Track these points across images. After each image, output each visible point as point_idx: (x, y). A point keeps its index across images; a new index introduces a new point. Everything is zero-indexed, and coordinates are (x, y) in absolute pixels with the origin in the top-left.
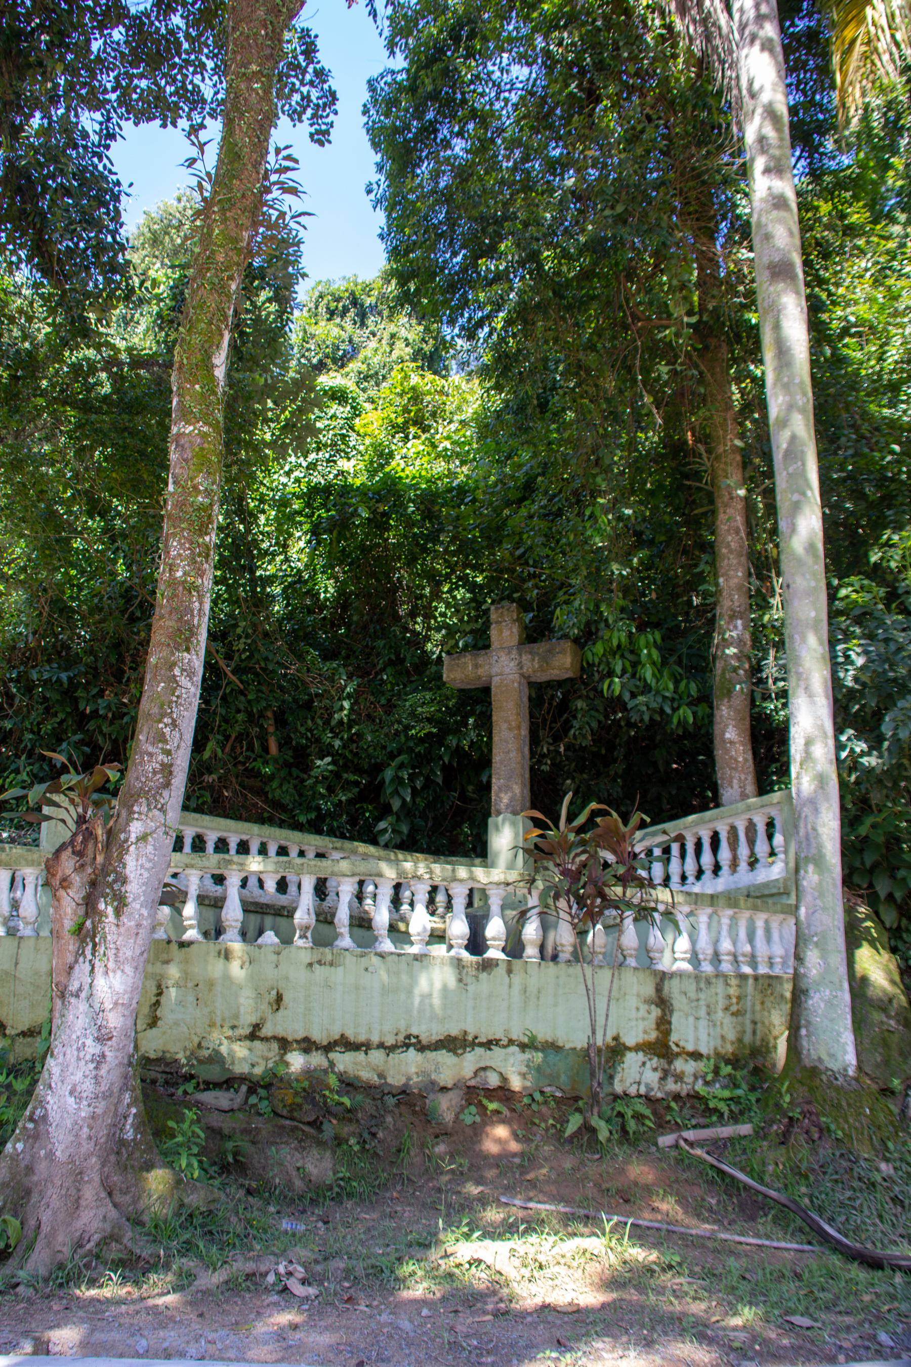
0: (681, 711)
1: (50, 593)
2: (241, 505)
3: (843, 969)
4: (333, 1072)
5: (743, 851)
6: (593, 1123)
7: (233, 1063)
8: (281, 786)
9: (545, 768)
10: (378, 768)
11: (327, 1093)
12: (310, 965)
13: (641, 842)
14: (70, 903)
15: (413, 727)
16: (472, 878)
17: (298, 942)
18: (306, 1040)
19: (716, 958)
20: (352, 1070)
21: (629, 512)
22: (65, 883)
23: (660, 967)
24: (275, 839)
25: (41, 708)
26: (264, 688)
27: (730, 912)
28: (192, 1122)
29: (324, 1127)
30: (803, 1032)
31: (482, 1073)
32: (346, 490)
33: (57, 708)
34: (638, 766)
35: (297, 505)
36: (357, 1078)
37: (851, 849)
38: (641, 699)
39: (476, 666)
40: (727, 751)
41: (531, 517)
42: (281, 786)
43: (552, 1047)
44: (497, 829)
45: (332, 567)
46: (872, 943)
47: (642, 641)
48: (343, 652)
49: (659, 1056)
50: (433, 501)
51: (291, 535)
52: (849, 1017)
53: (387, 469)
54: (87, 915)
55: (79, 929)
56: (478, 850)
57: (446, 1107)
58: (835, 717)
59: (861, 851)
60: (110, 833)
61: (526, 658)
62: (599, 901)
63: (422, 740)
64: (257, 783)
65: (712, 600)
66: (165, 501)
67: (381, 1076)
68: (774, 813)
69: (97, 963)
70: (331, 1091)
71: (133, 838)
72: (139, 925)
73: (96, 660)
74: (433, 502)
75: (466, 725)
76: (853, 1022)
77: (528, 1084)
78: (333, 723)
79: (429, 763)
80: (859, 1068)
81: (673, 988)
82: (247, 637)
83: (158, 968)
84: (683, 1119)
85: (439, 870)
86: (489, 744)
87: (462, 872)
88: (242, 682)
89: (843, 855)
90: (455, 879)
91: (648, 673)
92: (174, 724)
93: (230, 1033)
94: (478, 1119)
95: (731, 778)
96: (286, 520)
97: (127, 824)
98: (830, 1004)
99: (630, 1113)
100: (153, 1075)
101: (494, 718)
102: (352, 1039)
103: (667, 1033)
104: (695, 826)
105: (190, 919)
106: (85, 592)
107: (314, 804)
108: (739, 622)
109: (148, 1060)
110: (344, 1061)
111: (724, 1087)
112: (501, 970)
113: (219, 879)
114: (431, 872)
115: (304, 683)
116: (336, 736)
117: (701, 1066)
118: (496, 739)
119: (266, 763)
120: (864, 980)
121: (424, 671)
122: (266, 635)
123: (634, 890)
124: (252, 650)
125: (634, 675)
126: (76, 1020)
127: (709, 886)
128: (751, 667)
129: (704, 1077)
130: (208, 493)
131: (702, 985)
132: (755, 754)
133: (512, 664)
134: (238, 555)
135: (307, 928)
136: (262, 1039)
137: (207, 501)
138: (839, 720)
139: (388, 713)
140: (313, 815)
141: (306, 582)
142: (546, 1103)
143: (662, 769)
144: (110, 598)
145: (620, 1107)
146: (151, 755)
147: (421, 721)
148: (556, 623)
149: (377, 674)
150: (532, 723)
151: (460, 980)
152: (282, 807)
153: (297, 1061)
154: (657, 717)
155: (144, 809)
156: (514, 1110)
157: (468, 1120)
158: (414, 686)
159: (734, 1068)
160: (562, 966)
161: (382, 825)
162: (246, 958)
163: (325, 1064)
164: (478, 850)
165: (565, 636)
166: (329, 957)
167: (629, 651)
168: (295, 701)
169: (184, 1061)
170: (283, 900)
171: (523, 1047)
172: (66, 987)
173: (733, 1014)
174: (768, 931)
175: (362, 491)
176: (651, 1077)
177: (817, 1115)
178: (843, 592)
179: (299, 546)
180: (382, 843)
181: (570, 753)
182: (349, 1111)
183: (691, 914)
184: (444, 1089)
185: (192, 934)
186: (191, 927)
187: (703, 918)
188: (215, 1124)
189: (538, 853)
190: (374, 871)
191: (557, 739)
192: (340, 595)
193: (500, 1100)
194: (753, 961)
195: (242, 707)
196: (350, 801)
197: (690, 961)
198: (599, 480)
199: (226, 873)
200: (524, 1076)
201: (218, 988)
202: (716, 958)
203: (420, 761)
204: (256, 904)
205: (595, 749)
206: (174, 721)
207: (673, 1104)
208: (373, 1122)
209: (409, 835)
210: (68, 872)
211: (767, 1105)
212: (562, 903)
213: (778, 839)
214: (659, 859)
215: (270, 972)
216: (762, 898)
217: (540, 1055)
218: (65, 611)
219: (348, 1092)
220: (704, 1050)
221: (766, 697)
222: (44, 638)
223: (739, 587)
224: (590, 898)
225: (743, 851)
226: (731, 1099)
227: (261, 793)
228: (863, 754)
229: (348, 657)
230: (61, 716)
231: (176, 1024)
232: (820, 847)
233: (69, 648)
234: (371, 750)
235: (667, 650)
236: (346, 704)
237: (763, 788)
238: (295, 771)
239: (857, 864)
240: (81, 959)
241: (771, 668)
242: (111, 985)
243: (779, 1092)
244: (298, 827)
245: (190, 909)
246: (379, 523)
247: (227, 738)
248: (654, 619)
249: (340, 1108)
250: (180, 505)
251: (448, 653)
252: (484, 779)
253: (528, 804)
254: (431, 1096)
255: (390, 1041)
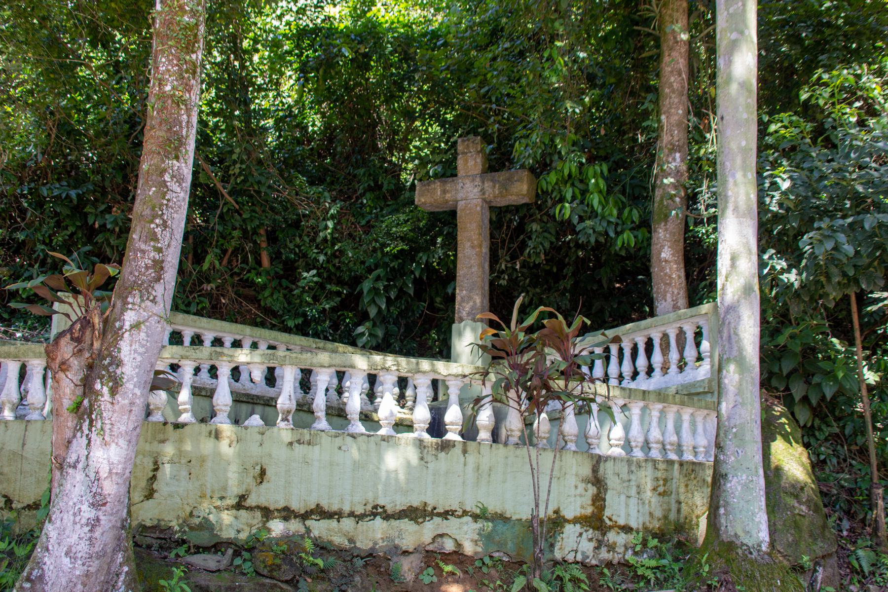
0: (625, 235)
1: (58, 116)
2: (235, 44)
3: (759, 458)
4: (309, 537)
5: (674, 355)
6: (535, 584)
7: (221, 530)
8: (272, 295)
9: (503, 282)
10: (357, 280)
11: (303, 555)
12: (291, 444)
13: (584, 346)
14: (69, 384)
15: (389, 245)
16: (434, 371)
17: (282, 424)
18: (286, 509)
19: (646, 446)
20: (325, 536)
21: (582, 55)
22: (64, 366)
23: (597, 451)
24: (265, 339)
25: (52, 223)
26: (257, 209)
27: (659, 406)
28: (180, 579)
29: (300, 585)
30: (722, 511)
31: (439, 540)
32: (331, 33)
33: (67, 222)
34: (585, 281)
35: (287, 46)
36: (330, 542)
37: (770, 355)
38: (588, 223)
39: (444, 192)
40: (662, 269)
41: (494, 59)
42: (272, 295)
43: (501, 518)
44: (460, 334)
45: (320, 103)
46: (786, 438)
47: (591, 172)
48: (328, 179)
49: (594, 529)
50: (408, 43)
51: (282, 74)
52: (763, 499)
53: (368, 15)
54: (84, 395)
55: (77, 408)
56: (445, 352)
57: (407, 568)
58: (759, 240)
59: (779, 359)
60: (106, 322)
61: (488, 185)
62: (544, 392)
63: (396, 257)
64: (251, 292)
65: (654, 135)
66: (153, 19)
67: (351, 541)
68: (701, 323)
69: (93, 436)
70: (307, 553)
71: (127, 326)
72: (132, 403)
73: (103, 180)
74: (409, 45)
75: (435, 244)
76: (767, 505)
77: (479, 549)
78: (319, 240)
79: (402, 277)
80: (772, 544)
81: (608, 470)
82: (242, 162)
83: (155, 447)
84: (615, 583)
85: (404, 364)
86: (454, 263)
87: (425, 364)
88: (237, 203)
89: (762, 361)
90: (418, 371)
91: (595, 200)
92: (165, 225)
93: (219, 503)
94: (435, 579)
95: (666, 292)
96: (278, 61)
97: (122, 314)
98: (746, 487)
99: (568, 577)
100: (149, 541)
101: (459, 238)
102: (326, 508)
103: (602, 508)
104: (633, 333)
105: (184, 404)
106: (90, 117)
107: (301, 311)
108: (678, 155)
109: (144, 527)
110: (319, 528)
111: (650, 558)
112: (458, 450)
113: (213, 371)
114: (398, 365)
115: (293, 205)
116: (321, 252)
117: (631, 538)
118: (459, 255)
119: (259, 274)
120: (778, 470)
121: (397, 196)
122: (260, 162)
123: (575, 383)
124: (247, 175)
125: (582, 202)
126: (75, 487)
127: (643, 383)
128: (687, 195)
129: (633, 548)
130: (194, 13)
131: (633, 468)
132: (688, 276)
133: (476, 190)
134: (234, 88)
135: (289, 412)
136: (247, 509)
137: (193, 21)
138: (764, 242)
139: (367, 233)
140: (300, 321)
141: (296, 116)
142: (494, 566)
143: (605, 286)
144: (115, 124)
145: (559, 572)
146: (143, 252)
147: (396, 239)
148: (515, 154)
149: (357, 198)
150: (492, 243)
151: (422, 459)
152: (274, 314)
153: (277, 527)
154: (602, 240)
155: (137, 300)
156: (466, 572)
157: (427, 580)
158: (389, 209)
159: (660, 542)
160: (511, 447)
161: (361, 329)
162: (234, 437)
163: (302, 530)
164: (445, 352)
165: (523, 166)
166: (307, 437)
167: (579, 180)
168: (286, 220)
169: (177, 528)
170: (270, 392)
171: (476, 517)
172: (64, 459)
173: (660, 494)
174: (693, 423)
175: (346, 35)
176: (587, 546)
177: (733, 584)
178: (773, 128)
179: (289, 83)
180: (360, 345)
181: (525, 270)
182: (322, 571)
183: (624, 407)
184: (406, 553)
185: (185, 417)
186: (185, 411)
187: (636, 410)
188: (203, 583)
189: (496, 353)
190: (348, 363)
191: (514, 258)
192: (326, 128)
193: (455, 563)
194: (679, 450)
195: (237, 225)
196: (333, 309)
197: (623, 448)
198: (557, 24)
199: (217, 364)
200: (476, 542)
201: (209, 464)
202: (646, 446)
203: (395, 275)
204: (248, 395)
205: (548, 268)
206: (165, 222)
207: (606, 571)
208: (343, 581)
209: (384, 339)
210: (67, 356)
211: (688, 574)
212: (512, 394)
213: (705, 345)
214: (599, 357)
215: (255, 450)
216: (691, 395)
217: (490, 524)
218: (71, 132)
219: (321, 555)
220: (634, 525)
221: (699, 222)
222: (54, 158)
223: (679, 124)
224: (537, 391)
225: (674, 355)
226: (657, 568)
227: (254, 300)
228: (783, 271)
229: (332, 183)
230: (71, 229)
231: (171, 495)
232: (741, 350)
233: (77, 168)
234: (351, 265)
235: (612, 182)
236: (330, 224)
237: (694, 300)
238: (285, 282)
239: (776, 369)
240: (79, 434)
241: (705, 197)
242: (107, 455)
243: (699, 563)
244: (287, 330)
245: (184, 395)
246: (361, 64)
247: (224, 252)
248: (602, 153)
249: (314, 569)
250: (168, 24)
251: (420, 180)
252: (450, 291)
253: (487, 307)
254: (395, 559)
255: (359, 510)
